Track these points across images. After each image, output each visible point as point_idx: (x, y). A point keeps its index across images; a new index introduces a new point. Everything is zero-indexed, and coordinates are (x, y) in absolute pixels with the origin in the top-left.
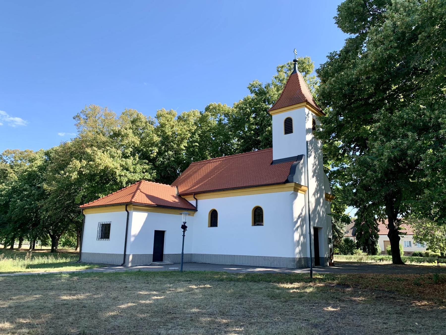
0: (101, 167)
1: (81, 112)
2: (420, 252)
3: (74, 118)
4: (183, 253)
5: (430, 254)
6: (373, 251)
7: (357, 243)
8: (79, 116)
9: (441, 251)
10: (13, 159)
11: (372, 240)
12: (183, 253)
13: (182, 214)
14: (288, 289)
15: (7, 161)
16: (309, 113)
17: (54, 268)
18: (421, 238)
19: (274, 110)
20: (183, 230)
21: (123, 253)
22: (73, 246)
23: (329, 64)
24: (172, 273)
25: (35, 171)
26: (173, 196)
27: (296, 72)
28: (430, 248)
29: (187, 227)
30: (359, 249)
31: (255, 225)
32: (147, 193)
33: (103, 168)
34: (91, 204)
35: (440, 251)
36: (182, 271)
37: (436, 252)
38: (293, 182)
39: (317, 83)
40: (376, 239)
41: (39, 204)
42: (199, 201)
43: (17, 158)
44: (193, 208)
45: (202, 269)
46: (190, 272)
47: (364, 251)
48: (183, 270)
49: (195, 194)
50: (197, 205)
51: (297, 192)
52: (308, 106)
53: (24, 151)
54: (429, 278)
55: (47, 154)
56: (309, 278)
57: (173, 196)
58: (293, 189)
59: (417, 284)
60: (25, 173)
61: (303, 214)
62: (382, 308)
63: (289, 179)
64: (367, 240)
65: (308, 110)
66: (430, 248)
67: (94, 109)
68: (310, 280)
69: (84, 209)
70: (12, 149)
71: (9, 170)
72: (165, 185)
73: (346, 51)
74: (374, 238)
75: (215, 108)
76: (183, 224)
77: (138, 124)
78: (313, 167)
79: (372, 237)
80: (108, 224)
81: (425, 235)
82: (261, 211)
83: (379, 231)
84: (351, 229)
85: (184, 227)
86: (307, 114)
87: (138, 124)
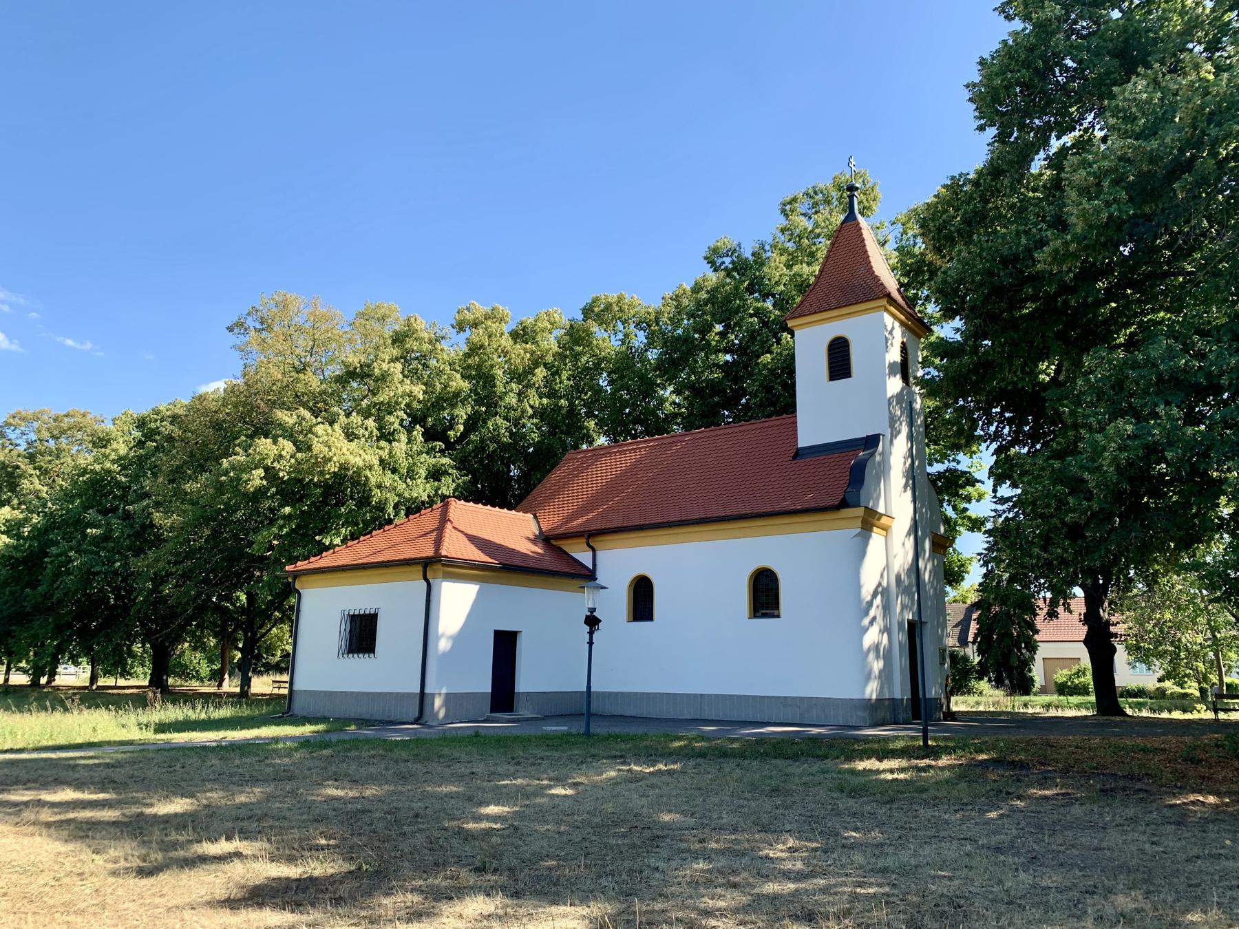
0: (332, 467)
1: (249, 314)
2: (1141, 685)
3: (230, 329)
4: (589, 687)
5: (1168, 692)
6: (1022, 685)
7: (979, 663)
8: (242, 325)
9: (1199, 683)
10: (33, 437)
11: (1019, 657)
12: (589, 687)
13: (583, 587)
14: (878, 772)
15: (18, 442)
16: (893, 328)
17: (241, 729)
18: (1149, 649)
19: (800, 316)
20: (587, 629)
21: (418, 691)
22: (193, 677)
23: (949, 204)
24: (549, 741)
25: (109, 472)
26: (528, 539)
27: (855, 219)
28: (1167, 676)
29: (600, 621)
30: (986, 679)
31: (755, 617)
32: (469, 532)
33: (336, 470)
34: (316, 563)
35: (1196, 685)
36: (588, 734)
37: (1186, 685)
38: (858, 506)
39: (886, 242)
40: (1030, 651)
41: (137, 564)
42: (599, 554)
43: (45, 435)
44: (587, 573)
45: (640, 730)
46: (610, 736)
47: (998, 683)
48: (592, 730)
49: (590, 536)
50: (594, 565)
51: (871, 531)
52: (892, 309)
53: (63, 413)
54: (1217, 746)
55: (141, 424)
56: (919, 748)
57: (528, 539)
58: (859, 523)
59: (1191, 760)
60: (83, 476)
61: (885, 583)
62: (1130, 812)
63: (850, 500)
64: (1007, 656)
65: (892, 319)
66: (1167, 676)
67: (284, 306)
68: (923, 753)
69: (297, 575)
70: (29, 410)
71: (24, 465)
72: (497, 509)
73: (994, 171)
74: (1024, 651)
75: (608, 307)
76: (589, 614)
77: (411, 344)
78: (905, 463)
79: (1020, 649)
80: (370, 615)
81: (1158, 643)
82: (772, 581)
83: (1037, 632)
84: (956, 626)
85: (592, 621)
86: (889, 329)
87: (411, 344)
